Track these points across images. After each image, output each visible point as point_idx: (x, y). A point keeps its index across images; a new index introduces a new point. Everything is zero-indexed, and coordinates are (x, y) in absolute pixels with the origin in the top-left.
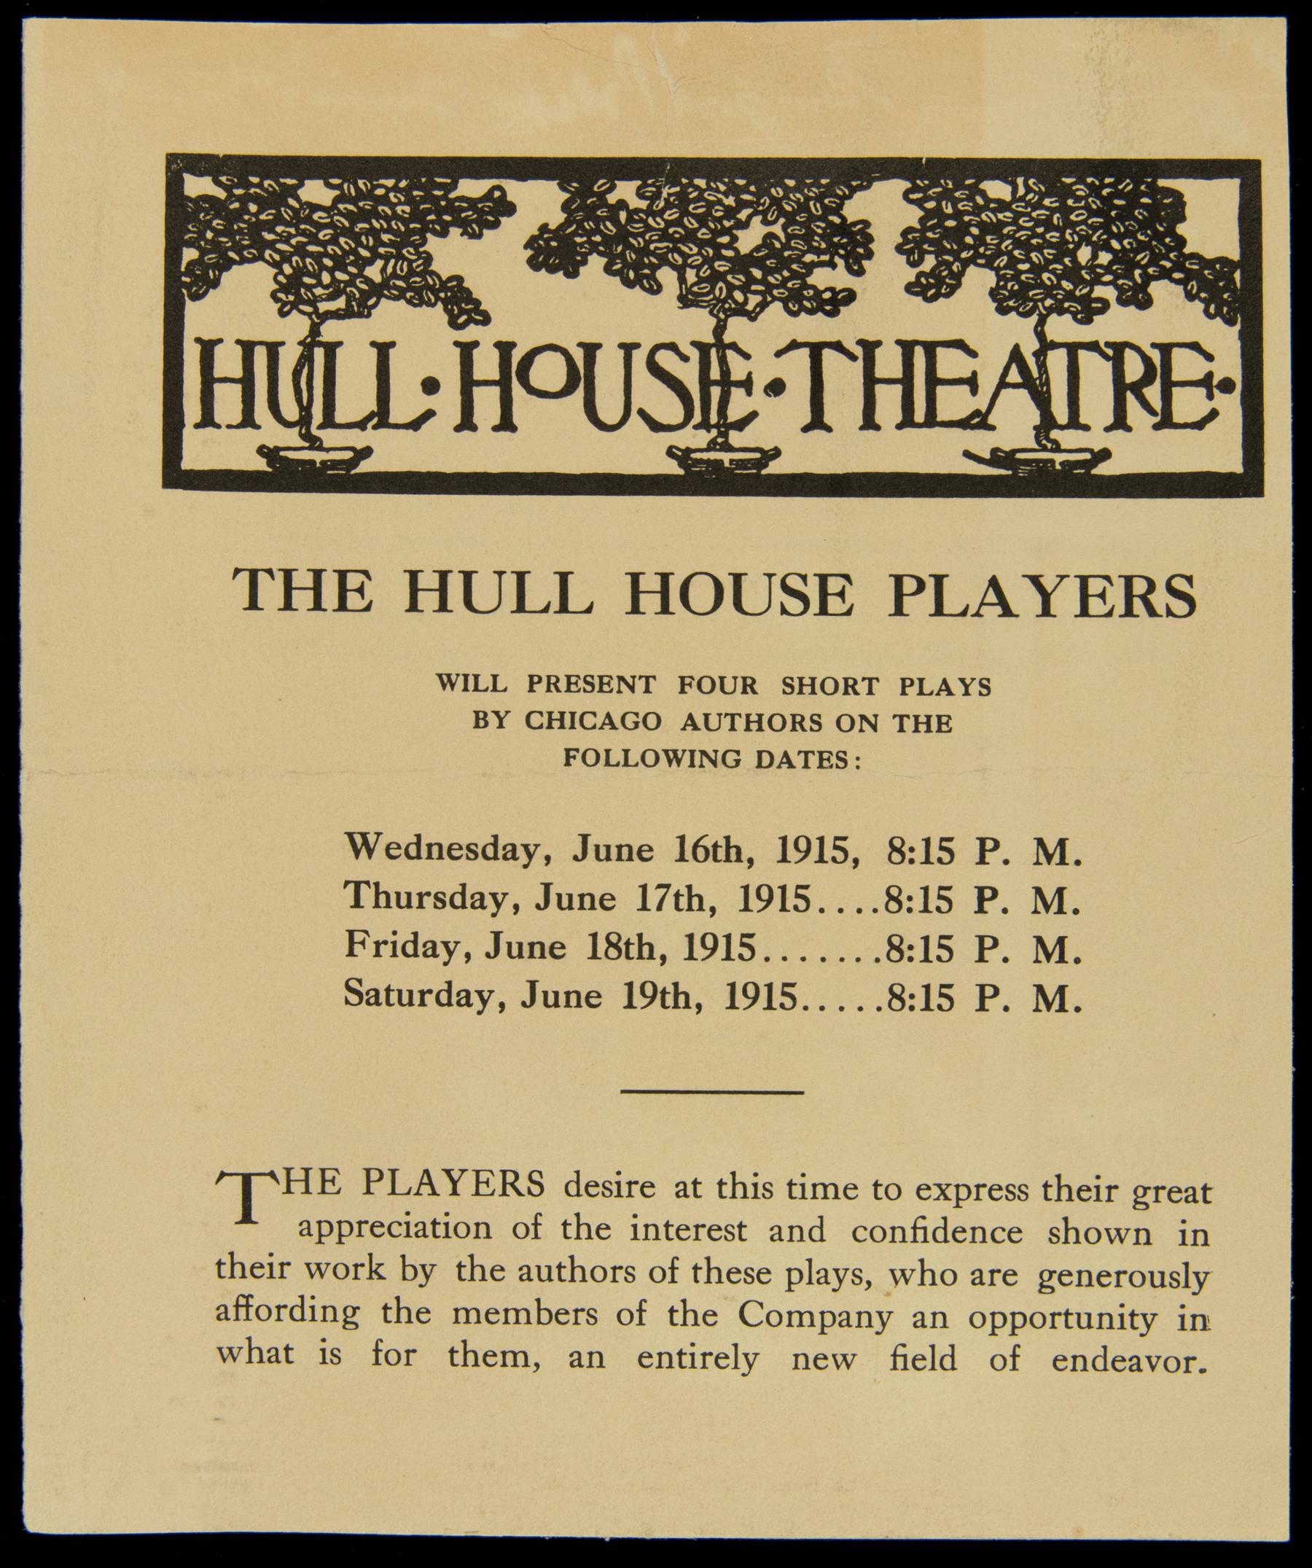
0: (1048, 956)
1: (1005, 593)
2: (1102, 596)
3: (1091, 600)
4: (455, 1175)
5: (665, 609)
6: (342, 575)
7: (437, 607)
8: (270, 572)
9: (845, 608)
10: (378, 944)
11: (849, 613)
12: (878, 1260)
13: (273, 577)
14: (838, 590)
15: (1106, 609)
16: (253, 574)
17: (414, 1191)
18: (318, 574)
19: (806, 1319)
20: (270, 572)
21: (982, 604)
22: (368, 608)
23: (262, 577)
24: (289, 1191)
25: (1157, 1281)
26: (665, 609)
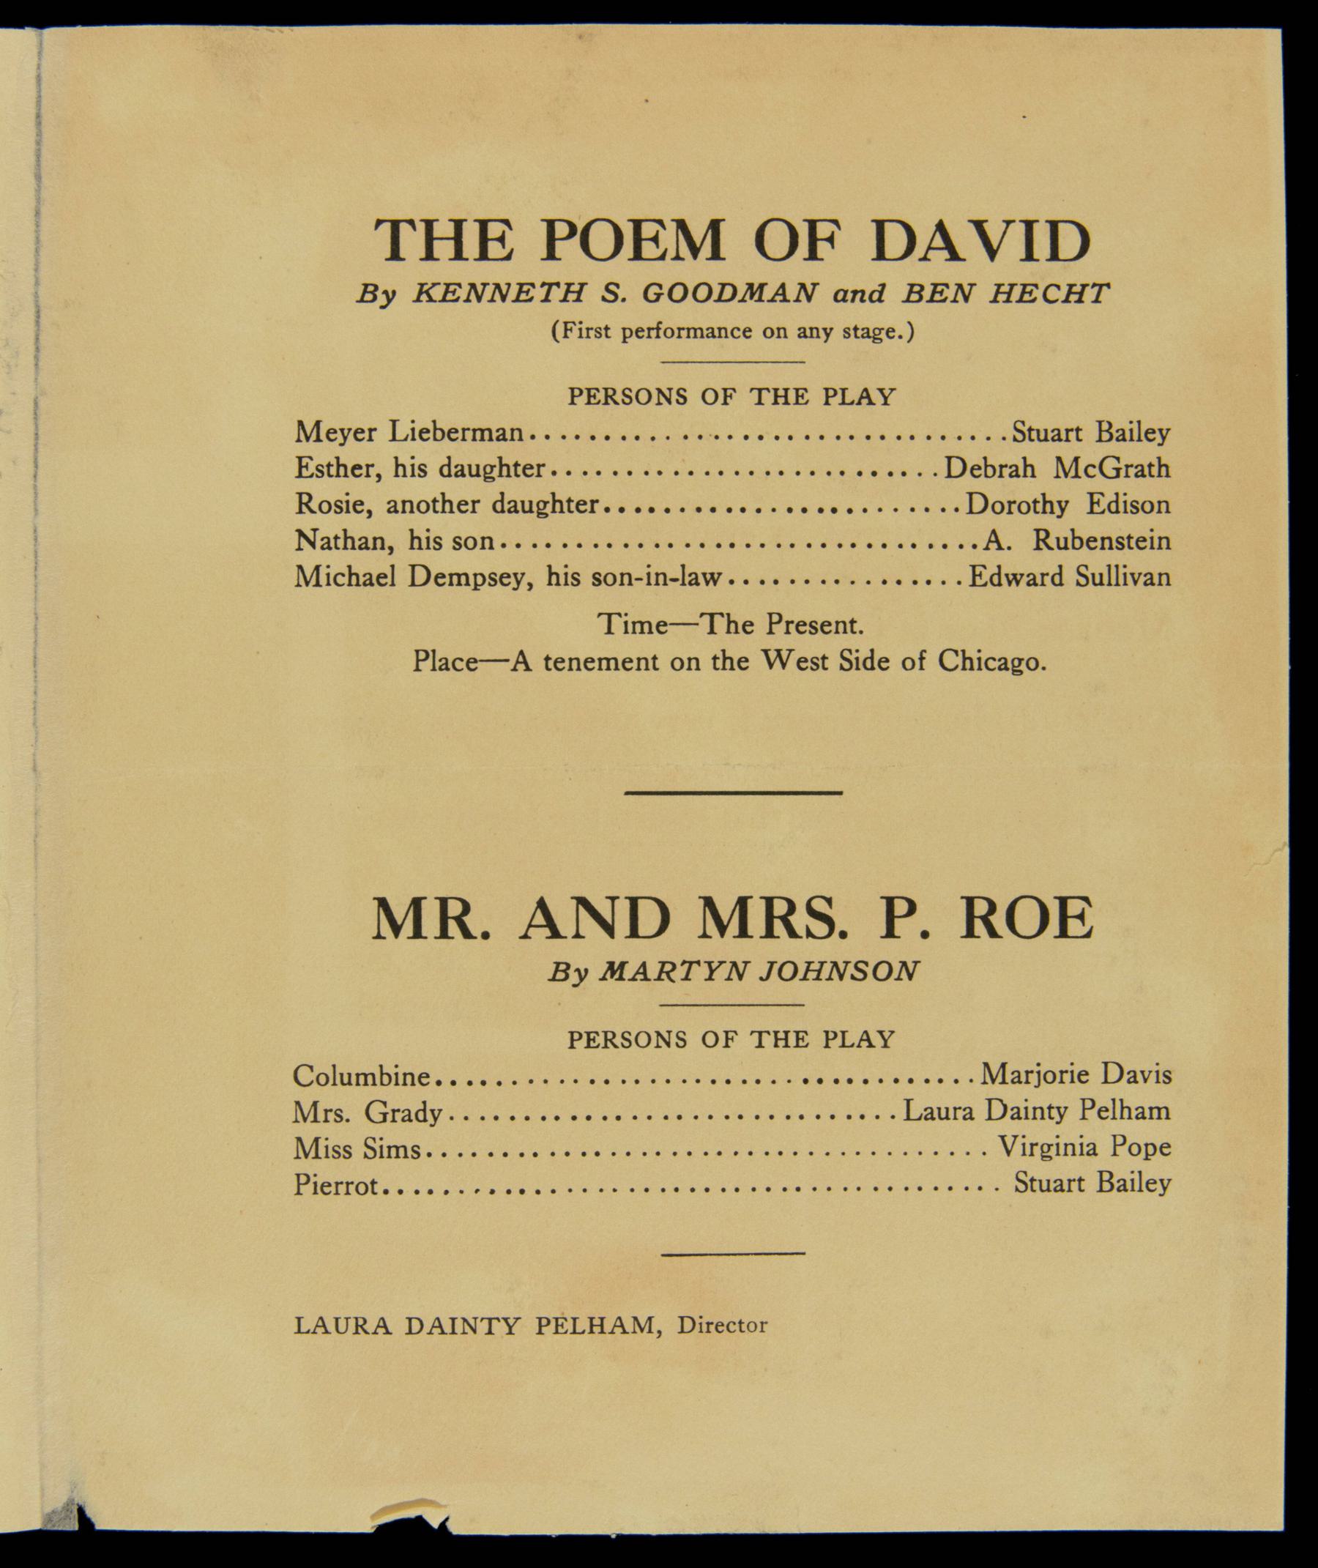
1: (389, 240)
2: (655, 239)
3: (644, 244)
6: (483, 225)
7: (452, 256)
8: (411, 222)
9: (505, 253)
11: (508, 257)
12: (395, 529)
13: (414, 228)
14: (498, 234)
15: (659, 253)
16: (395, 225)
18: (458, 224)
20: (411, 222)
21: (929, 248)
22: (508, 257)
23: (404, 228)
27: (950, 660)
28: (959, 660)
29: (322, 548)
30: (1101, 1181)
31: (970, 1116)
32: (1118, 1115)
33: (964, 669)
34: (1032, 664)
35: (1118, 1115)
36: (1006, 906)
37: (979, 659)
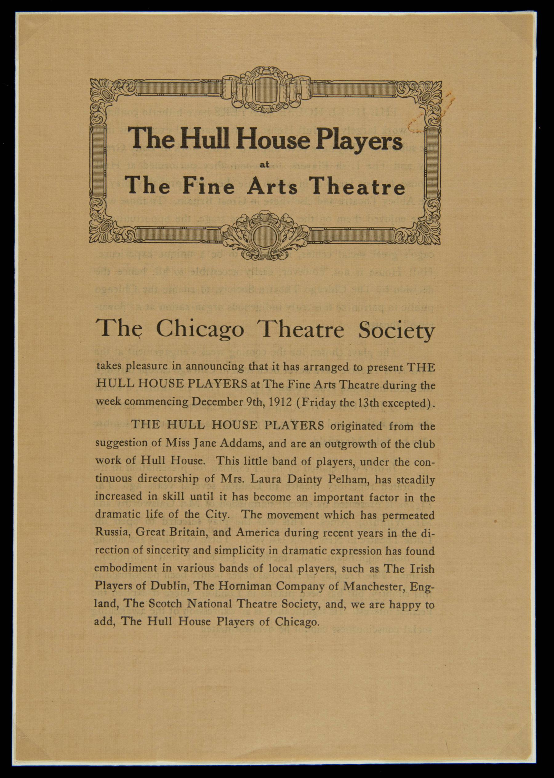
0: (348, 588)
4: (295, 423)
5: (220, 428)
10: (311, 402)
17: (281, 428)
19: (297, 587)
24: (149, 457)
25: (279, 143)
26: (220, 428)
27: (280, 622)
28: (283, 621)
29: (99, 606)
30: (172, 531)
31: (279, 480)
32: (345, 481)
33: (285, 625)
34: (314, 623)
35: (345, 481)
36: (159, 186)
37: (292, 621)
